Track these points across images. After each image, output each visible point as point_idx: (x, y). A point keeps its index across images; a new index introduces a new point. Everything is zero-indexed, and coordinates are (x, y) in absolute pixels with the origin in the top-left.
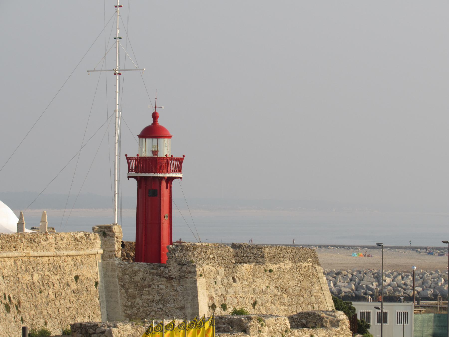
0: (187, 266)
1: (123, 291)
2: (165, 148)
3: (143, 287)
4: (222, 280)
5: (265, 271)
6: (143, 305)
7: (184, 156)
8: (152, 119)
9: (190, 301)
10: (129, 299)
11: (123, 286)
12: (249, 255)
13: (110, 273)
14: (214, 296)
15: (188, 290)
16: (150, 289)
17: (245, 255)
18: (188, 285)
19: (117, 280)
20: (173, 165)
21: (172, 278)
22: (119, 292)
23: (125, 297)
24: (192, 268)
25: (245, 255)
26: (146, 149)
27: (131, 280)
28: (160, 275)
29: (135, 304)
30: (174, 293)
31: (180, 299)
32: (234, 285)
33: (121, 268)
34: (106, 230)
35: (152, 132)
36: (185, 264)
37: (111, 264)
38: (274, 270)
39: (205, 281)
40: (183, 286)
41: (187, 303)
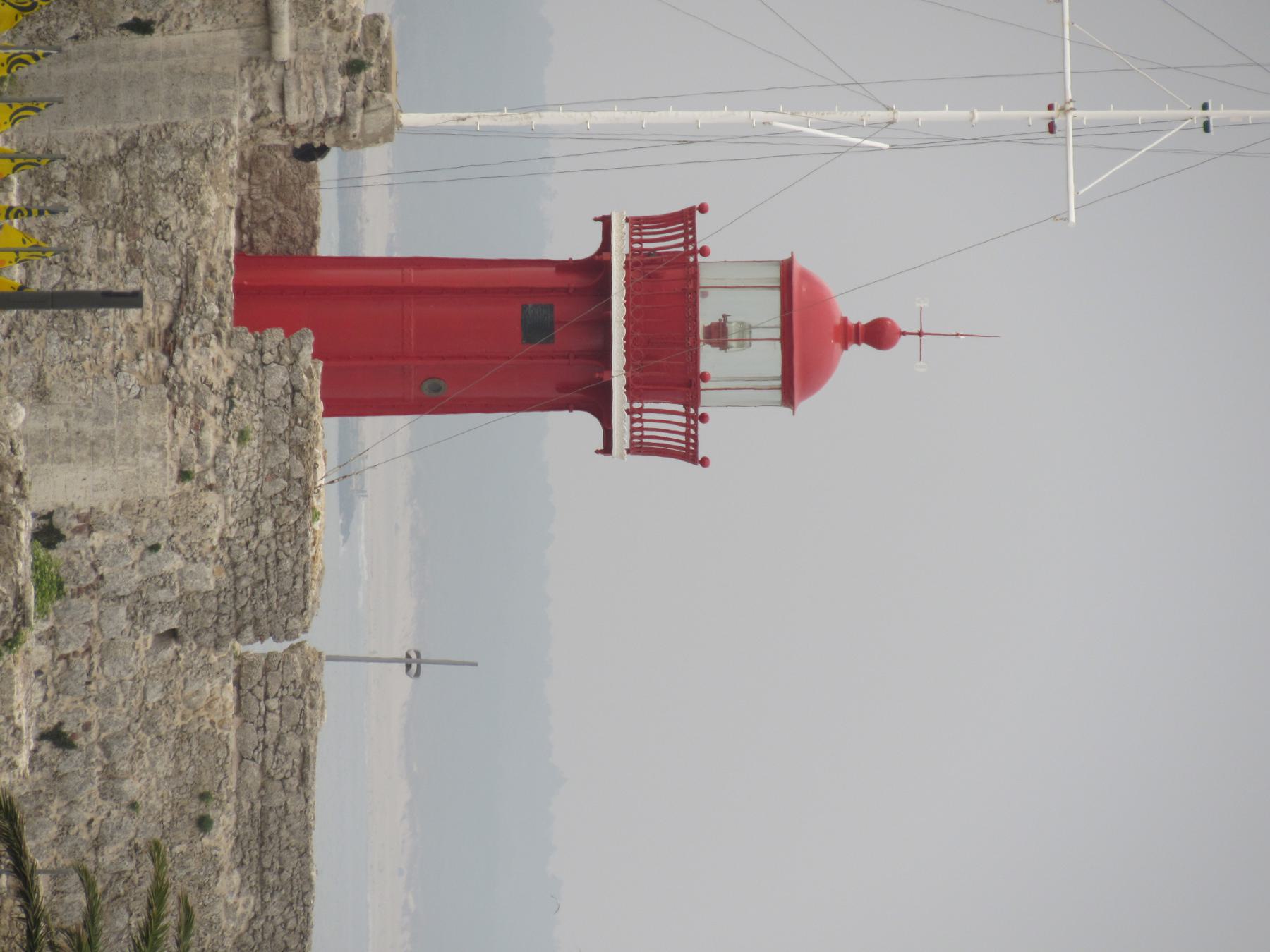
0: (225, 416)
1: (113, 147)
2: (737, 367)
3: (129, 229)
4: (165, 581)
5: (204, 797)
6: (53, 230)
7: (704, 462)
8: (860, 315)
9: (74, 428)
10: (76, 173)
11: (132, 145)
12: (274, 718)
13: (186, 90)
14: (98, 539)
15: (120, 418)
16: (122, 258)
17: (273, 704)
18: (143, 420)
19: (159, 120)
20: (665, 418)
21: (168, 352)
22: (109, 127)
23: (86, 153)
24: (216, 433)
25: (273, 704)
26: (733, 297)
27: (159, 180)
28: (180, 301)
29: (57, 199)
30: (108, 360)
31: (83, 385)
32: (146, 640)
33: (213, 137)
34: (373, 71)
35: (811, 339)
36: (232, 405)
37: (229, 93)
38: (206, 841)
39: (159, 494)
40: (138, 397)
41: (67, 414)
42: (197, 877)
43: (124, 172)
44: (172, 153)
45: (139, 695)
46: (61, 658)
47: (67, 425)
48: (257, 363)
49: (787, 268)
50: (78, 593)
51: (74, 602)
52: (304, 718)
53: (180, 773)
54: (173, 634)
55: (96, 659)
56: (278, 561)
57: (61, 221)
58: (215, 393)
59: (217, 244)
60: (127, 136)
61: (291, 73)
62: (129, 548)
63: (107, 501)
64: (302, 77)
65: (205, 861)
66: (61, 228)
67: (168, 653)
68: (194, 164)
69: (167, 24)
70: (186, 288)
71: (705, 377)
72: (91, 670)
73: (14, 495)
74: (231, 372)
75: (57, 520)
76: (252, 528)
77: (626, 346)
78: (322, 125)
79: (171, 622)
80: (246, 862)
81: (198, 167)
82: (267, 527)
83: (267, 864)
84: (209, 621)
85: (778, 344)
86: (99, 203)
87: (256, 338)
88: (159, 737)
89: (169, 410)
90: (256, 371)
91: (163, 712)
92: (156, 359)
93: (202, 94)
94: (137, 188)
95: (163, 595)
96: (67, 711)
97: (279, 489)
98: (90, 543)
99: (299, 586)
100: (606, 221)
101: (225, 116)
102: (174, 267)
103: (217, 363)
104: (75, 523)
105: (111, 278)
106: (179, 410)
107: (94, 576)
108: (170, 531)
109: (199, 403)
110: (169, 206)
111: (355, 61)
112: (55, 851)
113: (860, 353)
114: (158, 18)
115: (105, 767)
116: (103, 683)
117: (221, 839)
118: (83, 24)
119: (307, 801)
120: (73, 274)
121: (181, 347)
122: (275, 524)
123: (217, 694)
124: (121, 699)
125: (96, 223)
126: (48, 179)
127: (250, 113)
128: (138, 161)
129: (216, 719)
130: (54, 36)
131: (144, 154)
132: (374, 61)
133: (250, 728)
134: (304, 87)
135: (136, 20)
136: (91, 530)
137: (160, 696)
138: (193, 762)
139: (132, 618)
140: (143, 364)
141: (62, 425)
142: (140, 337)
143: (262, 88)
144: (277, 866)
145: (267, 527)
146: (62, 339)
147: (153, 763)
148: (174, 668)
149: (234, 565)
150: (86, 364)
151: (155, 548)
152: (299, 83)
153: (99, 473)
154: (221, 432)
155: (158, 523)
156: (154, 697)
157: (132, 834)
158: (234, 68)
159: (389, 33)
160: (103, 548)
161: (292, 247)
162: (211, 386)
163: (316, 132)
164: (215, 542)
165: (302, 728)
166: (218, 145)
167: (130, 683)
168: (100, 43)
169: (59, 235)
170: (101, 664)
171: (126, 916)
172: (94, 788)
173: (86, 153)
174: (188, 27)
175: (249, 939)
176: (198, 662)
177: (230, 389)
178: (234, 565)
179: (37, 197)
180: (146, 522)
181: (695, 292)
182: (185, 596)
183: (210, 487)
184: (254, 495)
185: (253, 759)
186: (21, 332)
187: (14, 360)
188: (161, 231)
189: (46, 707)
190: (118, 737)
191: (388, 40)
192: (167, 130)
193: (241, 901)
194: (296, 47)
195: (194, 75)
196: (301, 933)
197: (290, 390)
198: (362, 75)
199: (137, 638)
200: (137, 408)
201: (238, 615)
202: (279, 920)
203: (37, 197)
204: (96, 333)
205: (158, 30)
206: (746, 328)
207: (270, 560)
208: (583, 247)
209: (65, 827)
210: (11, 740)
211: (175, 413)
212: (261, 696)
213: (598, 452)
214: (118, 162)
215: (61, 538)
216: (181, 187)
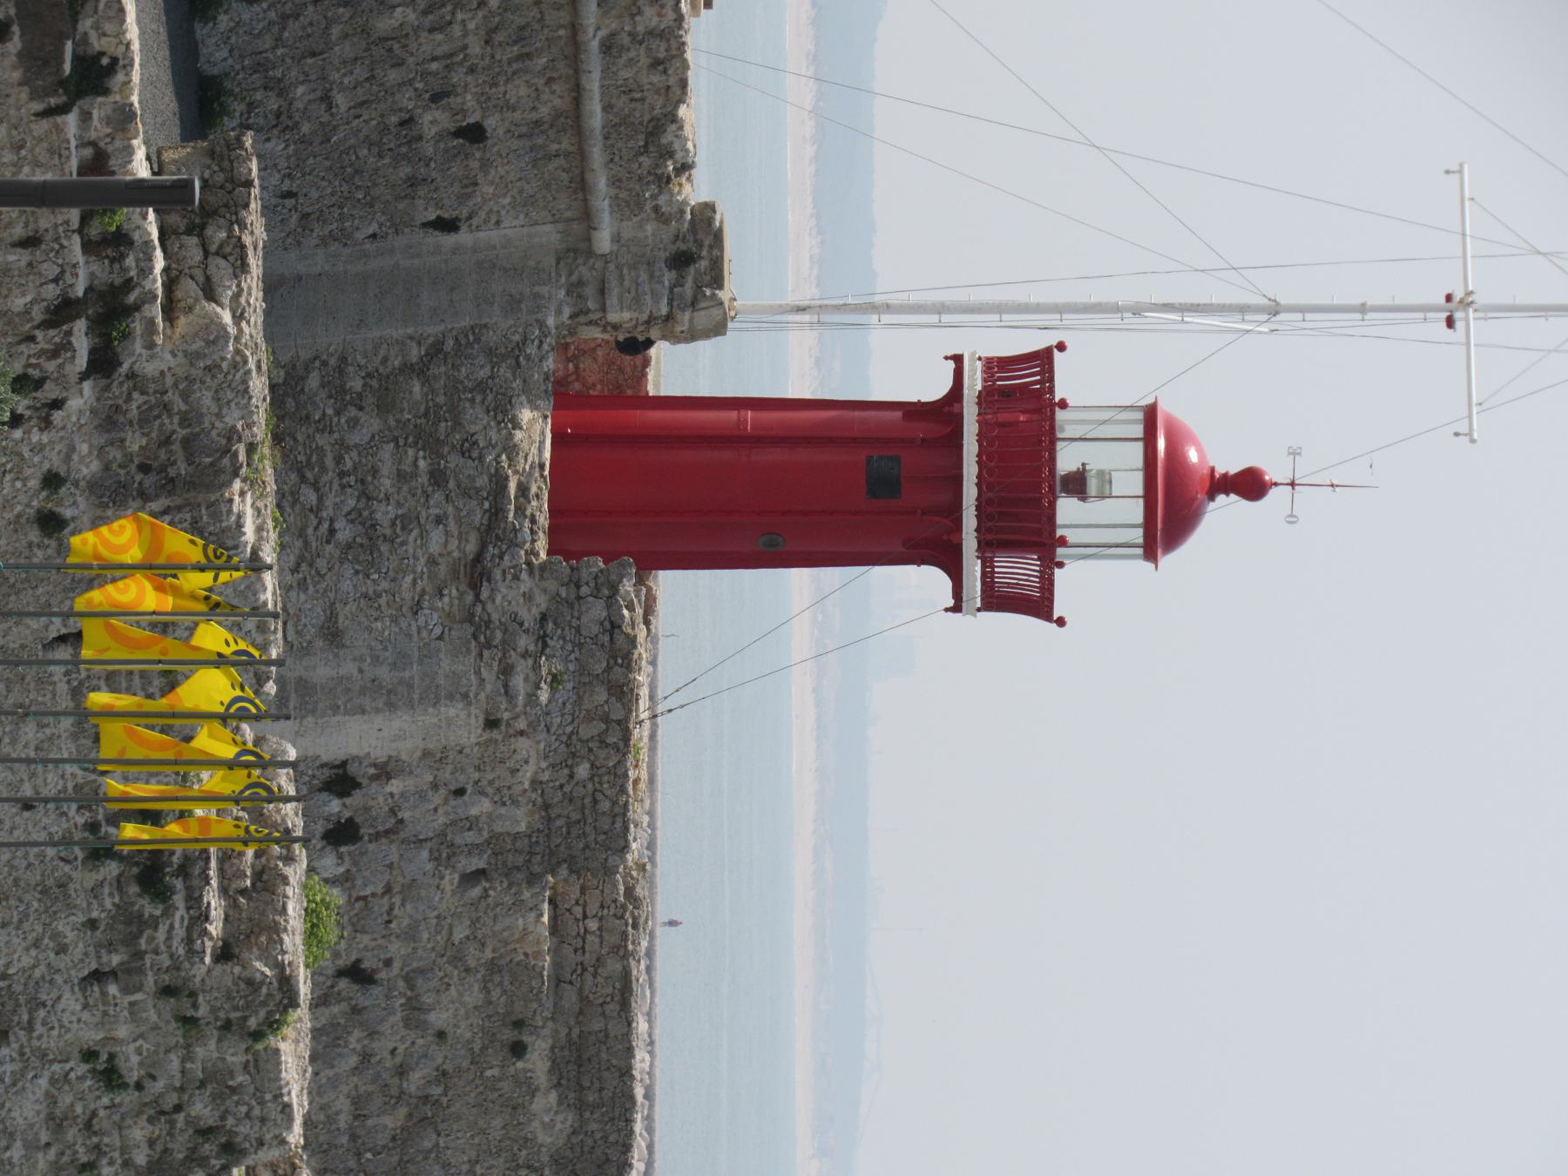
1: (415, 353)
3: (432, 445)
4: (472, 823)
5: (519, 1024)
6: (348, 448)
8: (1228, 464)
10: (374, 383)
11: (436, 350)
14: (395, 786)
15: (421, 662)
16: (424, 479)
18: (446, 663)
19: (466, 322)
20: (1017, 569)
21: (475, 586)
22: (410, 331)
23: (385, 360)
24: (526, 680)
25: (593, 925)
28: (490, 528)
29: (352, 412)
30: (407, 596)
31: (379, 624)
32: (450, 880)
36: (545, 645)
37: (544, 290)
38: (520, 1065)
39: (464, 741)
40: (440, 638)
41: (362, 659)
42: (509, 1099)
43: (426, 381)
44: (481, 359)
45: (445, 932)
46: (358, 899)
47: (361, 671)
48: (573, 596)
49: (1150, 415)
50: (377, 837)
51: (371, 847)
52: (626, 940)
53: (490, 1003)
54: (481, 873)
55: (397, 900)
56: (595, 801)
57: (356, 438)
58: (527, 631)
59: (530, 459)
60: (430, 341)
61: (612, 266)
62: (430, 793)
63: (407, 749)
64: (625, 271)
65: (518, 1083)
66: (356, 445)
67: (476, 892)
68: (504, 371)
69: (475, 222)
70: (497, 512)
71: (1063, 404)
72: (391, 909)
73: (280, 858)
74: (543, 607)
75: (352, 769)
76: (566, 771)
77: (978, 508)
78: (648, 322)
79: (478, 863)
80: (564, 1082)
81: (509, 375)
82: (583, 771)
83: (586, 1084)
84: (520, 860)
85: (1141, 501)
86: (398, 416)
87: (572, 569)
88: (467, 970)
89: (474, 652)
90: (571, 605)
91: (472, 949)
92: (461, 595)
93: (514, 292)
94: (441, 399)
95: (470, 837)
96: (366, 950)
97: (595, 732)
98: (388, 789)
99: (618, 825)
100: (958, 359)
101: (539, 316)
102: (481, 489)
103: (528, 597)
104: (372, 771)
105: (411, 502)
106: (486, 653)
107: (393, 821)
108: (477, 775)
109: (507, 645)
110: (476, 419)
111: (683, 253)
112: (355, 1079)
113: (1226, 507)
114: (465, 213)
115: (409, 999)
116: (406, 922)
117: (537, 1062)
118: (381, 225)
119: (629, 1024)
120: (369, 498)
121: (489, 581)
122: (592, 765)
123: (531, 928)
124: (425, 936)
125: (396, 440)
126: (342, 390)
127: (567, 311)
128: (443, 369)
129: (529, 951)
130: (349, 236)
131: (450, 361)
132: (704, 253)
133: (567, 950)
134: (626, 283)
135: (439, 218)
136: (389, 777)
137: (467, 932)
138: (504, 992)
139: (436, 859)
140: (446, 600)
141: (355, 673)
142: (443, 570)
143: (581, 283)
144: (597, 1085)
145: (583, 771)
146: (357, 572)
147: (461, 995)
148: (483, 904)
149: (546, 806)
150: (383, 601)
151: (460, 792)
152: (621, 278)
153: (396, 724)
154: (532, 677)
155: (462, 770)
156: (459, 934)
157: (440, 1061)
158: (550, 261)
159: (721, 222)
160: (402, 794)
161: (621, 378)
162: (521, 624)
163: (640, 328)
164: (527, 785)
165: (622, 952)
166: (531, 350)
167: (434, 921)
168: (400, 241)
169: (354, 454)
170: (403, 905)
171: (434, 1136)
172: (397, 1018)
173: (385, 360)
174: (498, 223)
175: (568, 1153)
176: (508, 900)
177: (542, 626)
178: (546, 806)
179: (330, 411)
180: (450, 768)
181: (1053, 441)
182: (495, 837)
183: (522, 733)
184: (569, 737)
185: (571, 983)
186: (311, 566)
187: (303, 597)
188: (468, 448)
189: (343, 944)
190: (421, 972)
191: (721, 230)
192: (477, 330)
193: (560, 1118)
194: (616, 239)
195: (506, 270)
196: (624, 1145)
197: (607, 625)
198: (692, 269)
199: (442, 878)
200: (439, 650)
201: (552, 853)
202: (598, 1136)
203: (330, 411)
204: (394, 565)
205: (464, 228)
206: (1105, 478)
207: (587, 801)
208: (931, 387)
209: (366, 1057)
210: (279, 1117)
211: (481, 655)
212: (580, 916)
213: (947, 610)
214: (420, 370)
215: (357, 785)
216: (490, 397)
